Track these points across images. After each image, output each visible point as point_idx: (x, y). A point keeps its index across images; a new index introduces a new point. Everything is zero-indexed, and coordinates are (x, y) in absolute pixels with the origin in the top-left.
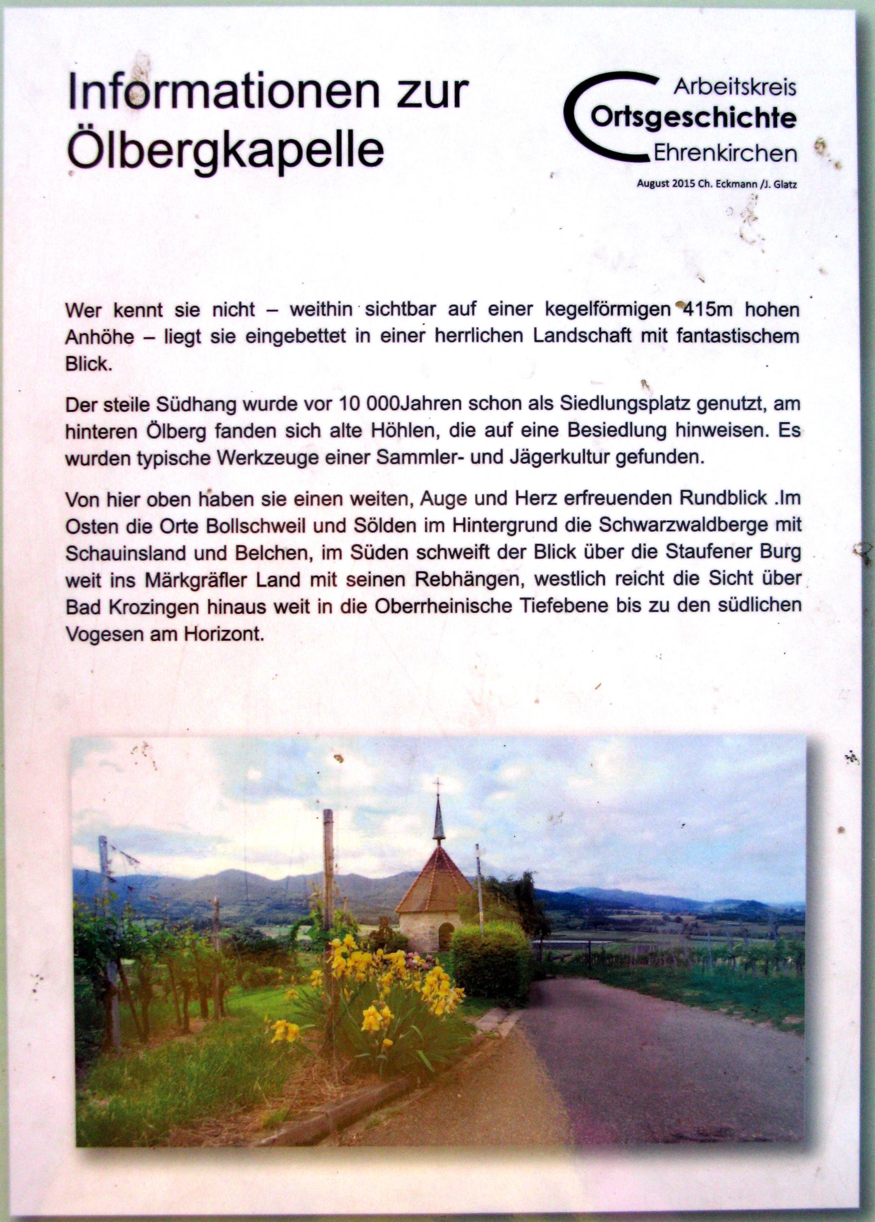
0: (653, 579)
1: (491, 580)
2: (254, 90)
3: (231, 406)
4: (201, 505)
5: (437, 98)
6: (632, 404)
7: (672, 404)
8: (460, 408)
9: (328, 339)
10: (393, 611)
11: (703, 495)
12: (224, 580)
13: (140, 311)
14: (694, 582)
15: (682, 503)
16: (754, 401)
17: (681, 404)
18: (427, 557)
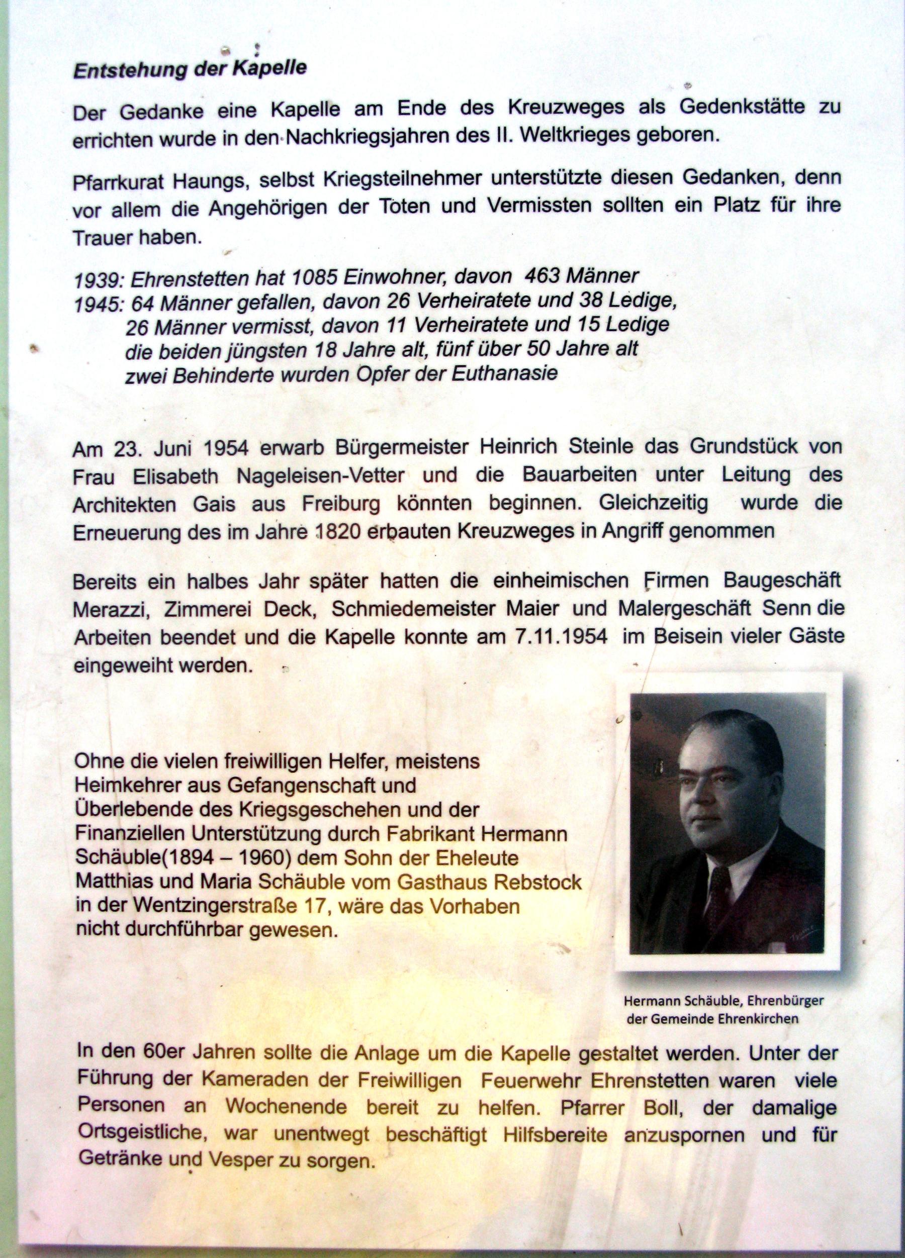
3: (176, 534)
7: (741, 206)
15: (496, 888)
16: (581, 175)
17: (751, 205)
18: (705, 614)
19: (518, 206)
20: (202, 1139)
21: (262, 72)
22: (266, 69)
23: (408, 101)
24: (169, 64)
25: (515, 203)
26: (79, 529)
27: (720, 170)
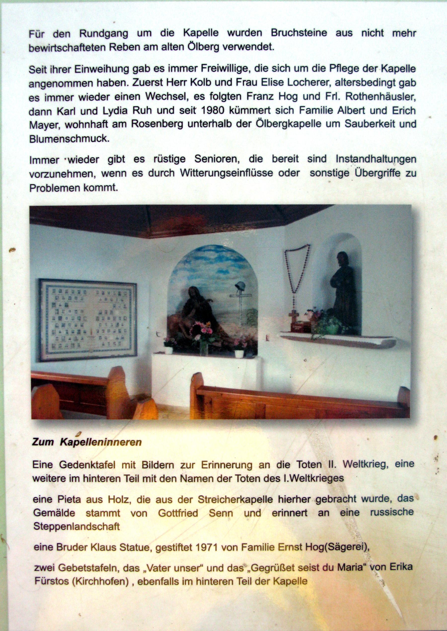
0: (378, 33)
1: (43, 84)
2: (335, 173)
4: (416, 172)
5: (52, 175)
6: (223, 174)
8: (126, 176)
9: (198, 174)
10: (364, 176)
11: (215, 176)
12: (248, 173)
13: (118, 173)
14: (357, 514)
19: (168, 465)
20: (150, 551)
21: (75, 444)
22: (77, 443)
23: (207, 461)
24: (42, 446)
25: (167, 464)
26: (395, 109)
27: (402, 495)
